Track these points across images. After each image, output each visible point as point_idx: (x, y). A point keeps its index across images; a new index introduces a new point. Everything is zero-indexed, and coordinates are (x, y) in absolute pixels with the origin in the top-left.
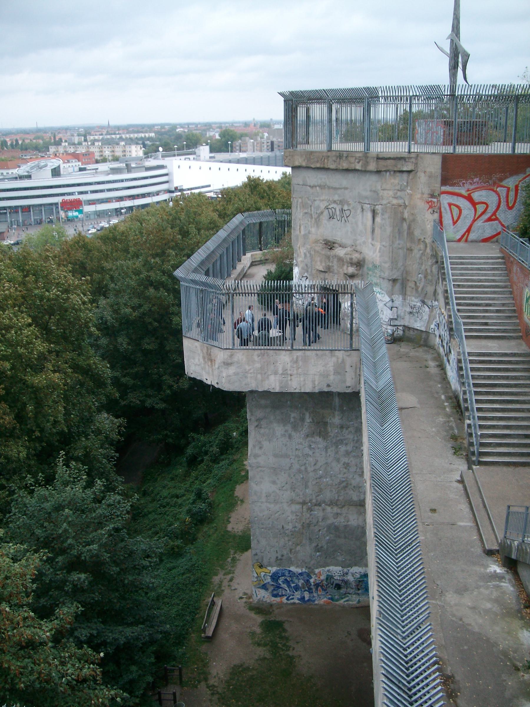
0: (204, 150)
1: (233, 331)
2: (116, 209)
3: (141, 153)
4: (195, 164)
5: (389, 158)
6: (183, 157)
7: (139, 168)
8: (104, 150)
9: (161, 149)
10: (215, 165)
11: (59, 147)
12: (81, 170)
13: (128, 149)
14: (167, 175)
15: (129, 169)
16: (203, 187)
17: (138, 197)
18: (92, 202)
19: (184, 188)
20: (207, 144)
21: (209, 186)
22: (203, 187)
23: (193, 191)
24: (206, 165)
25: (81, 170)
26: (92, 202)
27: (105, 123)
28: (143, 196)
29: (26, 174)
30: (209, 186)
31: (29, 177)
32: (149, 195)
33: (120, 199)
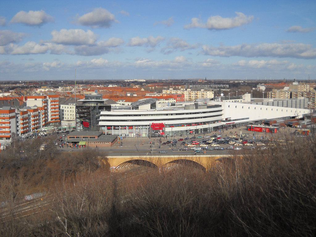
2: (186, 131)
4: (239, 105)
6: (234, 100)
8: (192, 93)
9: (222, 95)
10: (253, 106)
14: (221, 111)
15: (197, 106)
25: (173, 105)
27: (283, 117)
28: (204, 123)
30: (248, 118)
31: (137, 108)
32: (208, 122)
33: (189, 125)
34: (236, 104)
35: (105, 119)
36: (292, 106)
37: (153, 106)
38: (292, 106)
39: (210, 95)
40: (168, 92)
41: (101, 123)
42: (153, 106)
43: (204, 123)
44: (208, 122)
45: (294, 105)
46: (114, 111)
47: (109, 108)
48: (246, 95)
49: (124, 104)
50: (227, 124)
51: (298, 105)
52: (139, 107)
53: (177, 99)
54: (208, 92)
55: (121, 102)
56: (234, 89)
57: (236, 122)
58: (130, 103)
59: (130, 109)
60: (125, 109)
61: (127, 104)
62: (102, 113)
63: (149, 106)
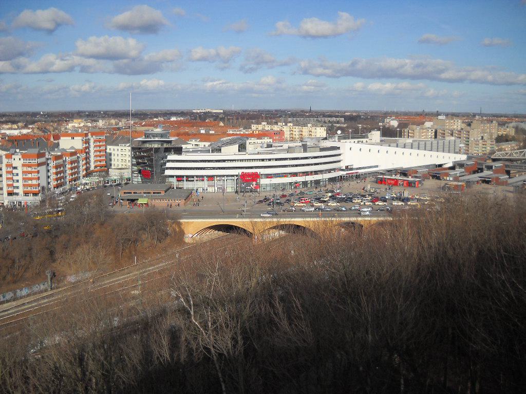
0: (376, 135)
1: (521, 181)
3: (324, 134)
4: (365, 147)
5: (156, 115)
6: (356, 140)
7: (315, 147)
10: (384, 148)
11: (259, 125)
12: (269, 146)
16: (360, 168)
17: (311, 173)
18: (269, 176)
19: (354, 167)
20: (379, 129)
21: (377, 166)
23: (360, 171)
24: (375, 148)
26: (269, 176)
28: (316, 173)
29: (218, 148)
33: (306, 174)
34: (360, 145)
35: (173, 166)
37: (242, 148)
39: (321, 132)
41: (167, 172)
43: (316, 173)
44: (321, 172)
45: (446, 149)
47: (179, 151)
51: (446, 149)
56: (355, 125)
58: (207, 144)
60: (201, 151)
61: (202, 144)
62: (170, 157)
63: (236, 147)
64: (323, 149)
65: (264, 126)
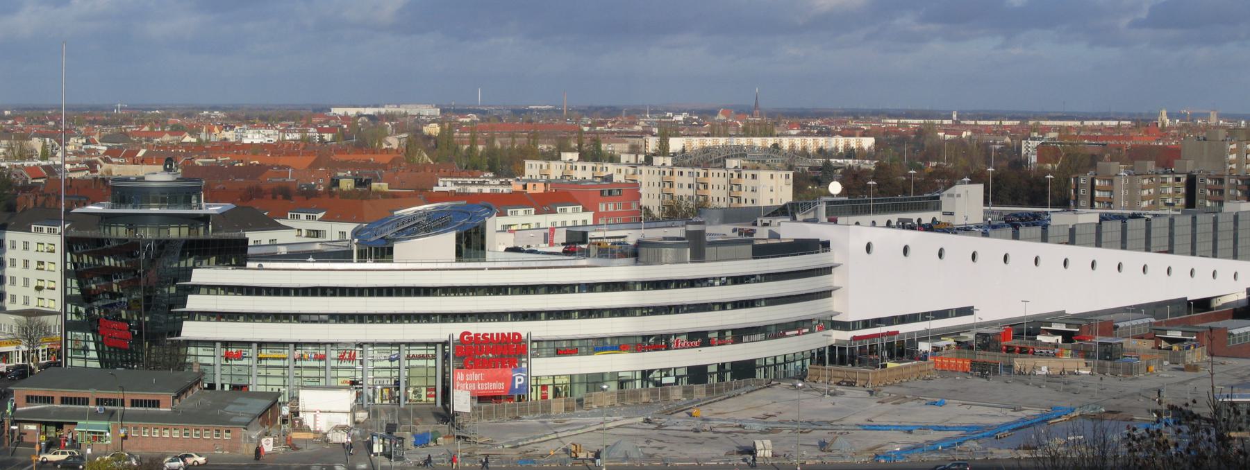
13: (746, 182)
14: (827, 270)
15: (698, 247)
16: (903, 319)
22: (903, 319)
30: (968, 311)
31: (384, 252)
33: (701, 338)
36: (1171, 244)
38: (1171, 244)
40: (555, 170)
41: (190, 330)
42: (471, 244)
46: (266, 265)
47: (234, 253)
48: (958, 189)
49: (317, 233)
50: (855, 338)
52: (398, 248)
53: (602, 208)
54: (764, 175)
55: (303, 223)
57: (904, 329)
59: (345, 256)
60: (321, 256)
62: (201, 276)
63: (447, 241)
64: (762, 252)
65: (572, 167)
